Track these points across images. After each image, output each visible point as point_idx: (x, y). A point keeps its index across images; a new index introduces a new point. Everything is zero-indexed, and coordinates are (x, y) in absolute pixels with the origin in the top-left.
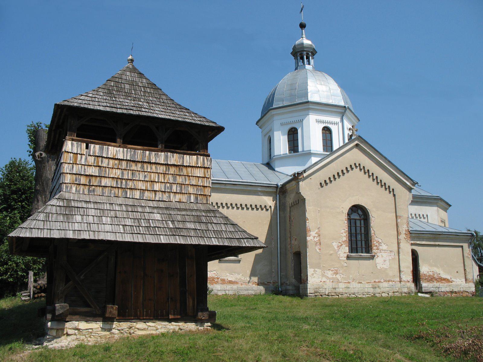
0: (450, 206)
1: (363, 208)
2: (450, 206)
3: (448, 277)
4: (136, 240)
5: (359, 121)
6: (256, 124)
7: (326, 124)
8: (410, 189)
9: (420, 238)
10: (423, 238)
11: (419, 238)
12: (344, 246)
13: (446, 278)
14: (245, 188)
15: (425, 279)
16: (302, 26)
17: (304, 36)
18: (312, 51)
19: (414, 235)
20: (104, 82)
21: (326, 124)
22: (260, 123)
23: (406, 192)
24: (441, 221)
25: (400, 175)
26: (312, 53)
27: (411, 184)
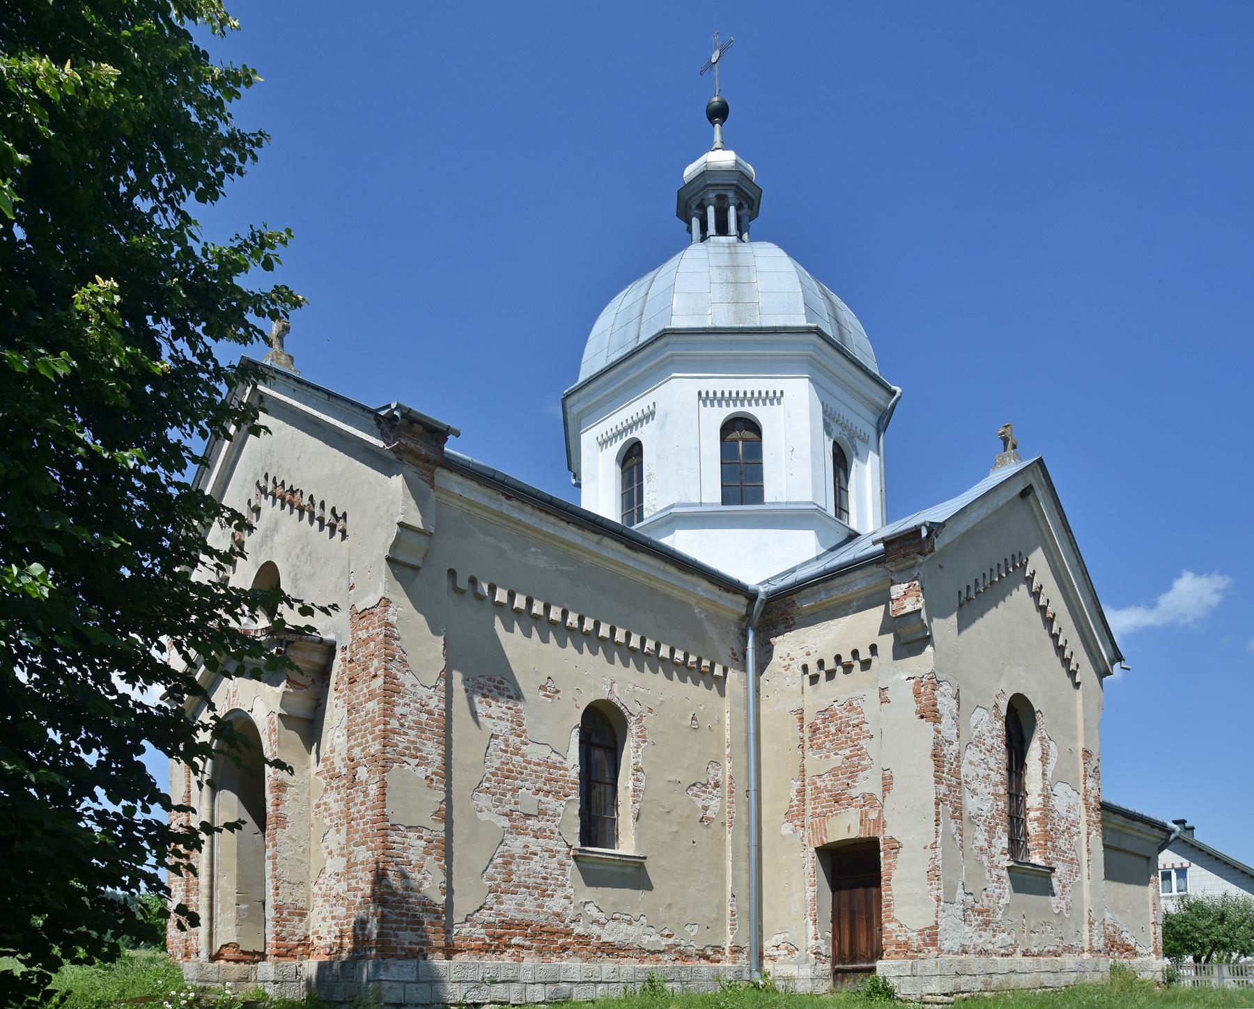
7: (735, 405)
16: (719, 113)
17: (718, 144)
21: (735, 405)
26: (739, 191)
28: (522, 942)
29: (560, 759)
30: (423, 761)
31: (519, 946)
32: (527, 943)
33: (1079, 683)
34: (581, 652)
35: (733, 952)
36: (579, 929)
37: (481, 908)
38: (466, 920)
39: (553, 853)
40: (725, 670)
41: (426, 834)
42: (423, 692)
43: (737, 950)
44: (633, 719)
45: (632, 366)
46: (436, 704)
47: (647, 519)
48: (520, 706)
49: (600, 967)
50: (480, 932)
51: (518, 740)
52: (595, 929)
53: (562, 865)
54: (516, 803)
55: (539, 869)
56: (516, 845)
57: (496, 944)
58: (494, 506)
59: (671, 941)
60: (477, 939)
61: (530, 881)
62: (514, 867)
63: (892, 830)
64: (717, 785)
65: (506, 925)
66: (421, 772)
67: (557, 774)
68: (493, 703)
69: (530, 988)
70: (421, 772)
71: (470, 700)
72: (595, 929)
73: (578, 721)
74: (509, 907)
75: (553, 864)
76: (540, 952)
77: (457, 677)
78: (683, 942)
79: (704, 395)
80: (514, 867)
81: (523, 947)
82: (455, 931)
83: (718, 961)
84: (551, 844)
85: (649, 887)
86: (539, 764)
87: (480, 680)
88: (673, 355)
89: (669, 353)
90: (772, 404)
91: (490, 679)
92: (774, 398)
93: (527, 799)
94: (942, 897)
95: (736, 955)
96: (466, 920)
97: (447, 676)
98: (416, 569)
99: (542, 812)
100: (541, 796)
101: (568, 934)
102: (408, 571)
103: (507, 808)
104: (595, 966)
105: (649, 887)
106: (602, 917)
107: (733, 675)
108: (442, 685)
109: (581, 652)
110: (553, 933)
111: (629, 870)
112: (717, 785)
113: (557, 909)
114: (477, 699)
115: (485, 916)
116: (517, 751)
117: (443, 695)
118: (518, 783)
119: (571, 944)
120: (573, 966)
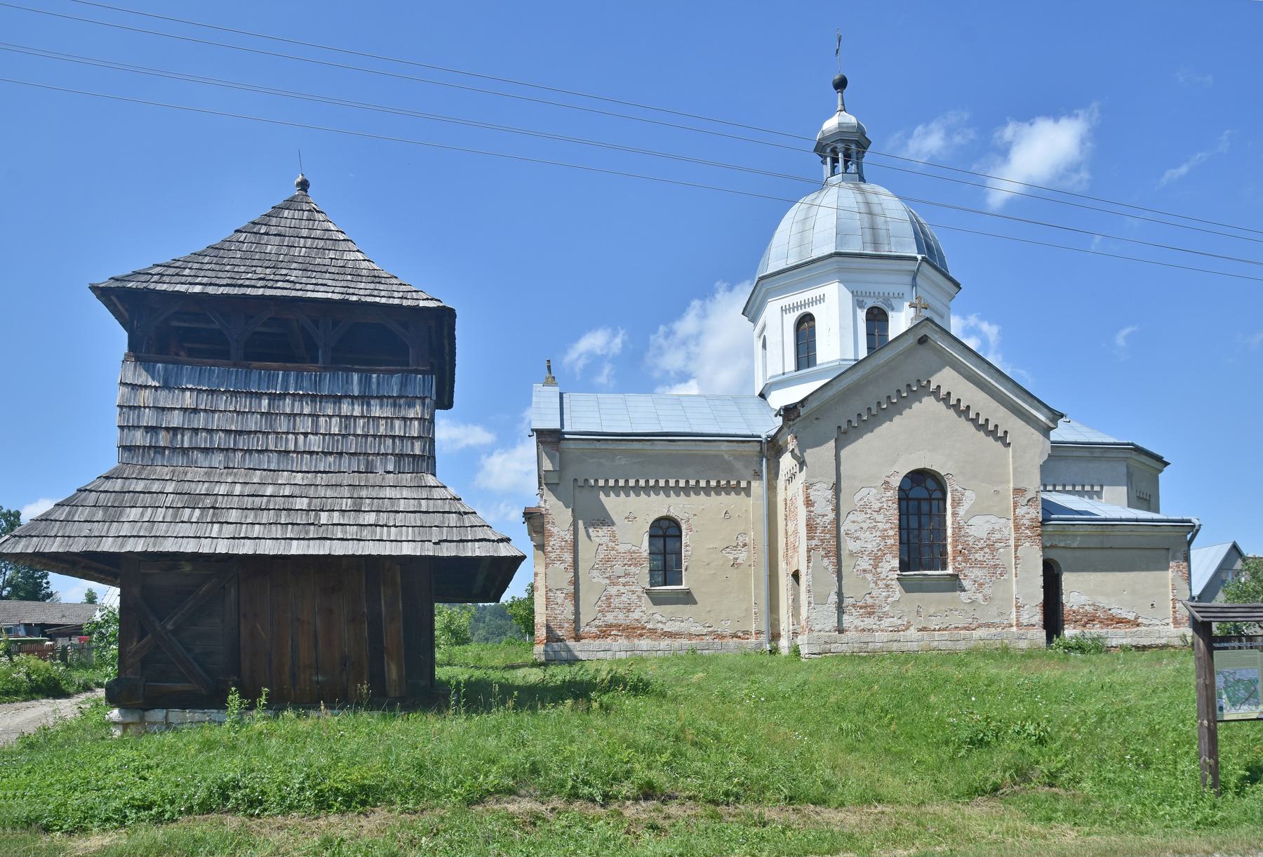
0: (1166, 464)
1: (937, 476)
2: (1166, 464)
3: (1131, 617)
4: (311, 552)
5: (957, 285)
6: (743, 314)
8: (1046, 431)
9: (1067, 535)
10: (1073, 535)
11: (1063, 535)
12: (889, 557)
13: (1126, 619)
14: (588, 447)
15: (1076, 622)
18: (857, 139)
19: (1051, 530)
20: (189, 254)
21: (801, 309)
22: (746, 313)
23: (1037, 436)
24: (1139, 498)
25: (1024, 401)
26: (858, 143)
27: (1048, 418)
28: (616, 633)
29: (637, 548)
30: (563, 562)
31: (615, 635)
32: (620, 634)
33: (1009, 444)
34: (649, 496)
35: (756, 634)
36: (649, 626)
37: (595, 619)
38: (587, 625)
39: (633, 592)
40: (749, 483)
41: (565, 591)
42: (562, 534)
43: (759, 633)
44: (683, 521)
45: (809, 270)
46: (569, 537)
47: (820, 365)
48: (614, 528)
49: (660, 644)
50: (594, 630)
51: (613, 544)
52: (660, 625)
53: (639, 597)
54: (613, 572)
55: (626, 600)
56: (613, 590)
57: (604, 633)
58: (593, 447)
59: (710, 629)
60: (593, 633)
61: (621, 606)
62: (612, 600)
63: (800, 569)
64: (745, 545)
65: (611, 626)
66: (562, 566)
67: (635, 556)
68: (600, 530)
69: (617, 653)
70: (562, 566)
71: (587, 532)
72: (660, 625)
73: (648, 529)
74: (610, 618)
75: (634, 597)
76: (627, 637)
77: (581, 523)
78: (719, 630)
79: (784, 308)
80: (612, 600)
81: (618, 635)
82: (582, 630)
83: (748, 639)
84: (633, 588)
85: (695, 603)
86: (625, 553)
87: (593, 522)
88: (767, 289)
89: (765, 289)
90: (820, 303)
91: (598, 520)
92: (821, 299)
93: (619, 569)
94: (813, 602)
95: (758, 635)
96: (587, 625)
97: (575, 524)
98: (558, 484)
99: (627, 575)
100: (626, 567)
101: (643, 629)
102: (554, 486)
103: (608, 575)
104: (657, 643)
105: (695, 603)
106: (664, 620)
107: (754, 484)
108: (572, 528)
109: (649, 496)
110: (634, 629)
111: (681, 596)
112: (745, 545)
113: (636, 617)
114: (591, 530)
115: (597, 622)
116: (613, 549)
117: (572, 532)
118: (614, 563)
119: (645, 633)
120: (644, 643)
